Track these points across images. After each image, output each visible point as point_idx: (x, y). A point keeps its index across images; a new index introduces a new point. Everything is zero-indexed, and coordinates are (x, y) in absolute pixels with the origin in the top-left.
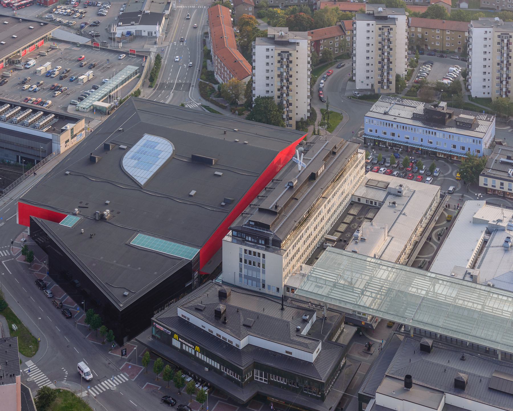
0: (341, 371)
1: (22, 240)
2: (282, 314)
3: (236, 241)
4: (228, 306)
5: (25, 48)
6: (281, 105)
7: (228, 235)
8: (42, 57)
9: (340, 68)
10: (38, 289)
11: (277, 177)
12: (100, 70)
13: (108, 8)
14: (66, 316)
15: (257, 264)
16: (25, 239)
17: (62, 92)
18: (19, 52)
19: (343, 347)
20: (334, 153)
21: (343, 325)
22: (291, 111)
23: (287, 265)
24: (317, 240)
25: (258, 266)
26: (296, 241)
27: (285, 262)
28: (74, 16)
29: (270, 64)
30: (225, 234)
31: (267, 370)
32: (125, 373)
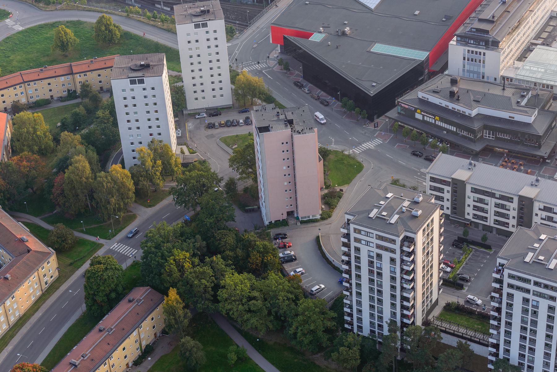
0: (552, 129)
1: (275, 56)
2: (503, 93)
3: (460, 44)
4: (459, 88)
10: (297, 89)
14: (324, 104)
15: (478, 61)
19: (554, 113)
21: (552, 101)
23: (503, 61)
24: (525, 44)
26: (510, 43)
27: (502, 58)
30: (451, 39)
31: (494, 130)
32: (379, 138)
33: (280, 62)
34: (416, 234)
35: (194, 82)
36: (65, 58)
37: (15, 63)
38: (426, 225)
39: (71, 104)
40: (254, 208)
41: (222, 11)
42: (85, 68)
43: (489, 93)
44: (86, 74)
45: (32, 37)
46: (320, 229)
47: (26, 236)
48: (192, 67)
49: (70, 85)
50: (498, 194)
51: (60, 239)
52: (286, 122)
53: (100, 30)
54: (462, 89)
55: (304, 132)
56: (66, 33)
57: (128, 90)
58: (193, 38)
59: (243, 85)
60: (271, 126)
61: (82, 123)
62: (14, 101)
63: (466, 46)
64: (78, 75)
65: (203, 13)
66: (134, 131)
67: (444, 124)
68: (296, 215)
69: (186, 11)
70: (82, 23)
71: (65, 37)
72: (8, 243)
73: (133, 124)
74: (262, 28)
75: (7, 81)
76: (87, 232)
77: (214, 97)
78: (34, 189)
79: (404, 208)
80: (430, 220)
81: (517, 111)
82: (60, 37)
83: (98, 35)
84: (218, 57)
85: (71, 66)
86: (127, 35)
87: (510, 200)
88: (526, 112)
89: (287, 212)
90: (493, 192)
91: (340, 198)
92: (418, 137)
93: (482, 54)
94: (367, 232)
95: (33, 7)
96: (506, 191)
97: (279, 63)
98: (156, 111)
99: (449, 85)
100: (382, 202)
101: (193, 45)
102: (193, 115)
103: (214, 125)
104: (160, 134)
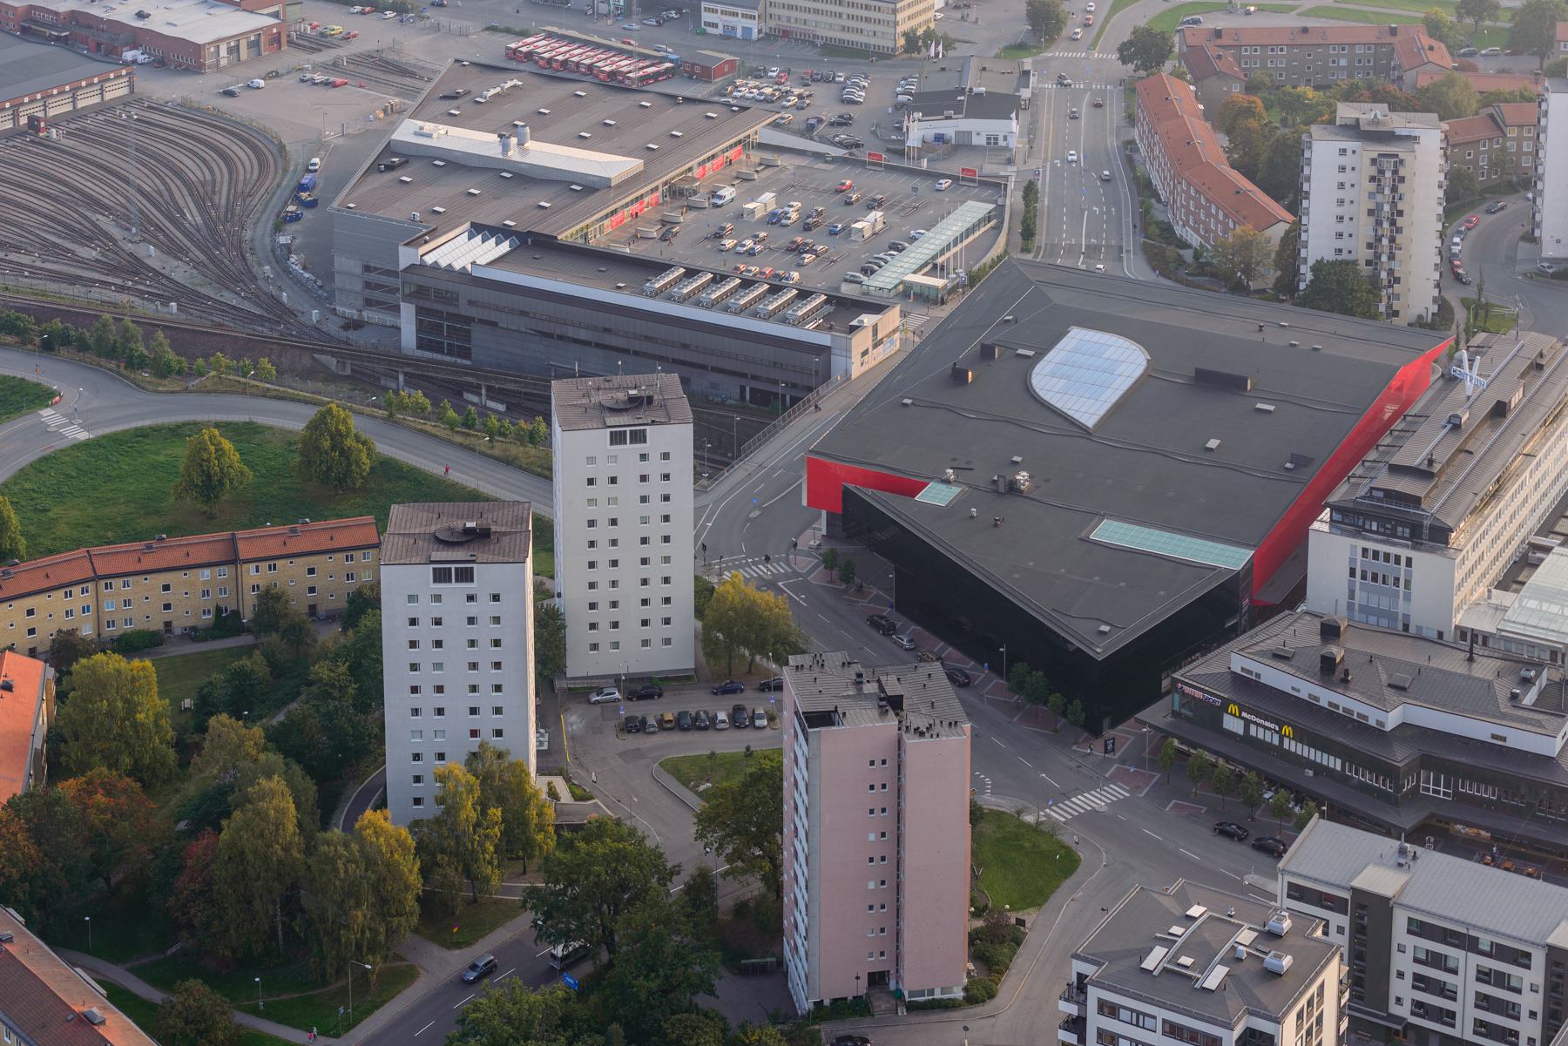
1: (812, 543)
2: (1470, 669)
5: (704, 162)
6: (1374, 281)
7: (1321, 521)
8: (746, 184)
9: (1494, 213)
10: (877, 636)
11: (1414, 410)
12: (897, 213)
13: (864, 87)
14: (958, 681)
15: (1391, 581)
16: (818, 542)
17: (818, 256)
18: (690, 169)
20: (1540, 367)
22: (1397, 297)
24: (1515, 544)
25: (1394, 584)
26: (1477, 536)
27: (1459, 575)
28: (784, 103)
29: (1347, 186)
33: (830, 561)
34: (1279, 1023)
35: (593, 596)
36: (207, 521)
37: (62, 529)
38: (1303, 1001)
39: (222, 650)
40: (766, 963)
41: (686, 400)
42: (273, 547)
43: (1432, 668)
44: (275, 565)
45: (114, 459)
46: (966, 1029)
47: (98, 1008)
48: (593, 555)
49: (225, 593)
50: (1485, 942)
51: (192, 1026)
52: (884, 703)
53: (317, 448)
54: (1354, 651)
55: (934, 732)
56: (220, 451)
57: (425, 599)
58: (602, 472)
59: (731, 613)
60: (840, 711)
61: (255, 700)
62: (60, 631)
63: (1357, 538)
64: (252, 566)
65: (636, 403)
66: (428, 720)
67: (1306, 748)
68: (892, 986)
69: (587, 395)
70: (259, 430)
71: (216, 462)
72: (43, 1027)
73: (428, 700)
74: (773, 469)
75: (48, 570)
76: (267, 1014)
77: (645, 643)
78: (114, 880)
79: (1241, 948)
80: (1314, 989)
81: (1513, 721)
82: (203, 460)
83: (309, 462)
84: (666, 529)
85: (233, 539)
86: (388, 469)
87: (1521, 958)
88: (1539, 724)
89: (869, 974)
90: (1472, 933)
91: (1019, 944)
92: (1232, 784)
93: (1403, 561)
94: (1138, 1013)
95: (120, 380)
96: (1508, 932)
97: (824, 561)
98: (497, 665)
99: (1316, 640)
100: (1176, 930)
101: (602, 489)
102: (582, 693)
103: (644, 722)
104: (499, 733)
